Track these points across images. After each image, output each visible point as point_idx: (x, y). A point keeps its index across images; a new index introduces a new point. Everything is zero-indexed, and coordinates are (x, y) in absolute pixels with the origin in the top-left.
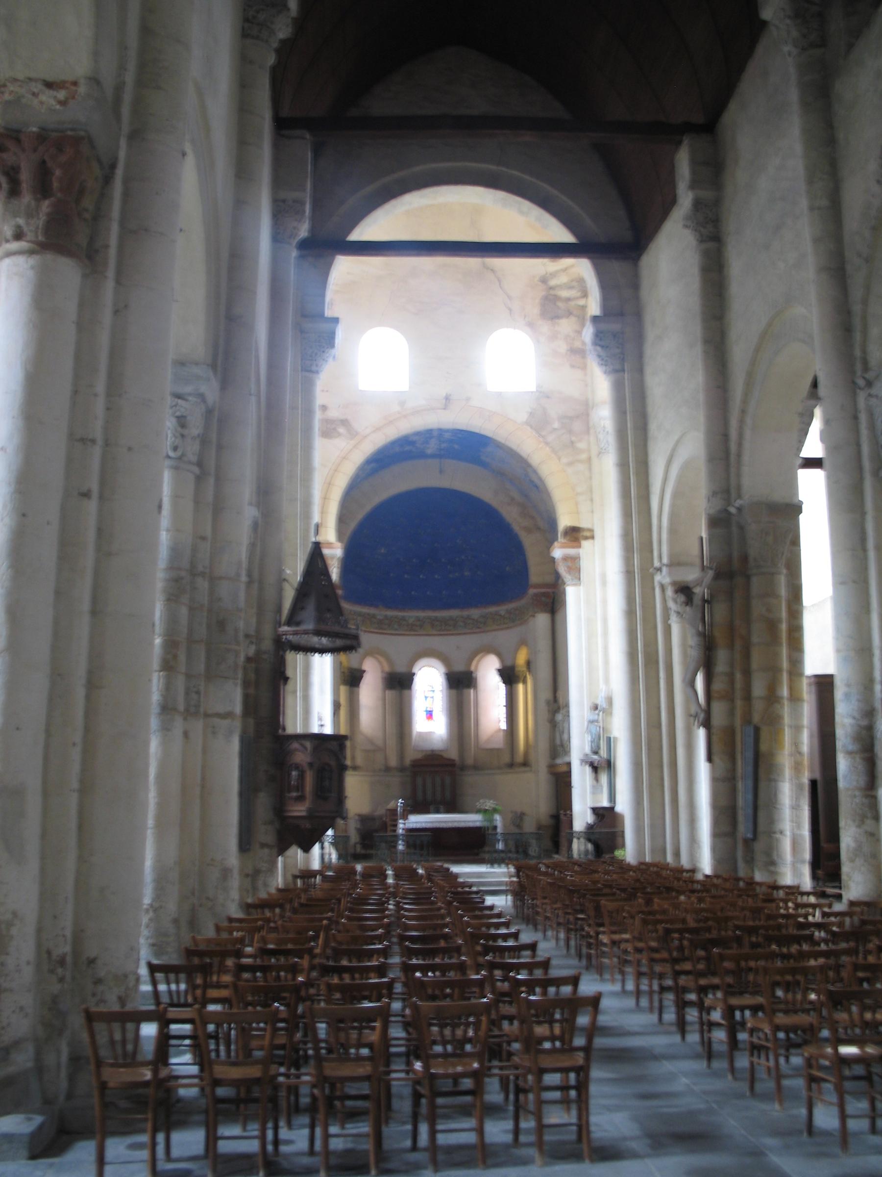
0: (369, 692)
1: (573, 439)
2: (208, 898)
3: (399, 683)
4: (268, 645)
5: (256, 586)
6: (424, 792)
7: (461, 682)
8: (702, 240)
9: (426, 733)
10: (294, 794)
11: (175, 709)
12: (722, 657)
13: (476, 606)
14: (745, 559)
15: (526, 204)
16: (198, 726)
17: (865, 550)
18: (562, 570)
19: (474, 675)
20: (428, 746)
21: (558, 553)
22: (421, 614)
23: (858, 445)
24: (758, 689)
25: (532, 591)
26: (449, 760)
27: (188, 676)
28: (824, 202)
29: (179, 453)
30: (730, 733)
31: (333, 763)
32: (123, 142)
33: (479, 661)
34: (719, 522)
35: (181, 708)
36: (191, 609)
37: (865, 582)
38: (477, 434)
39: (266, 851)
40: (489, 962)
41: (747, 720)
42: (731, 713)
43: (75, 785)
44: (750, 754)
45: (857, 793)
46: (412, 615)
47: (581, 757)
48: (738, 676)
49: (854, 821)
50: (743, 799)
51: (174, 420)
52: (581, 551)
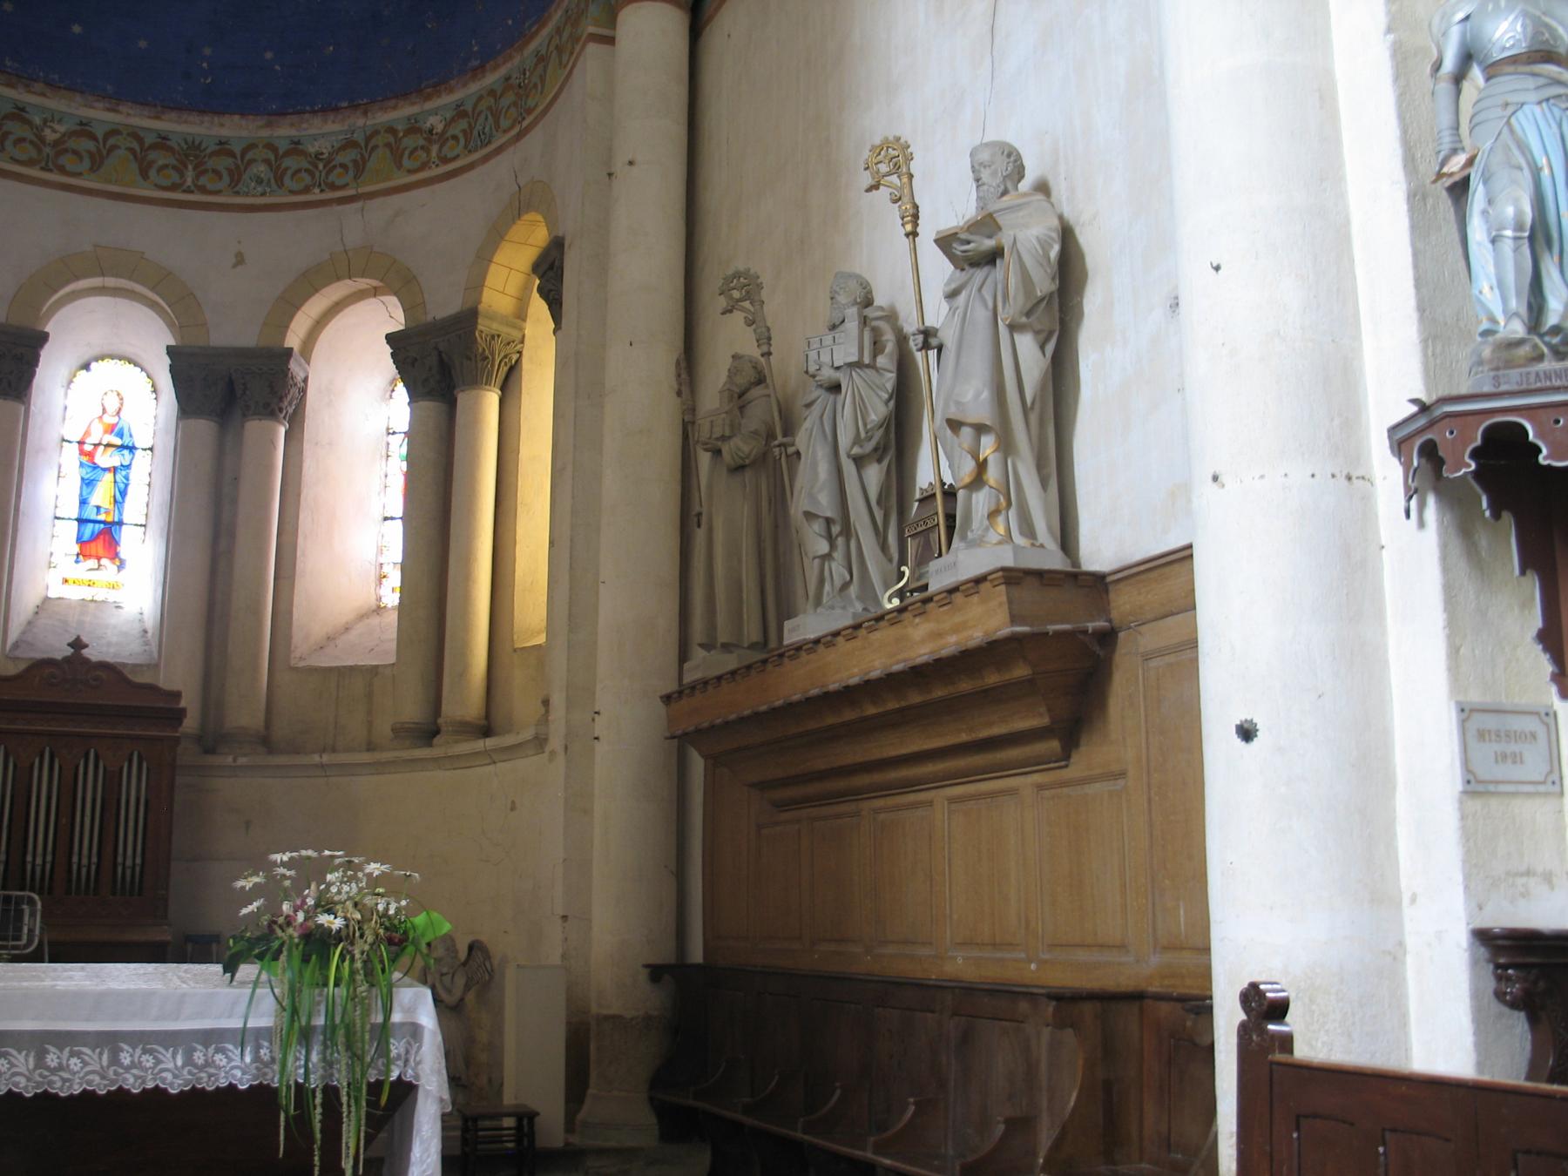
7: (236, 393)
13: (329, 109)
22: (100, 115)
26: (153, 689)
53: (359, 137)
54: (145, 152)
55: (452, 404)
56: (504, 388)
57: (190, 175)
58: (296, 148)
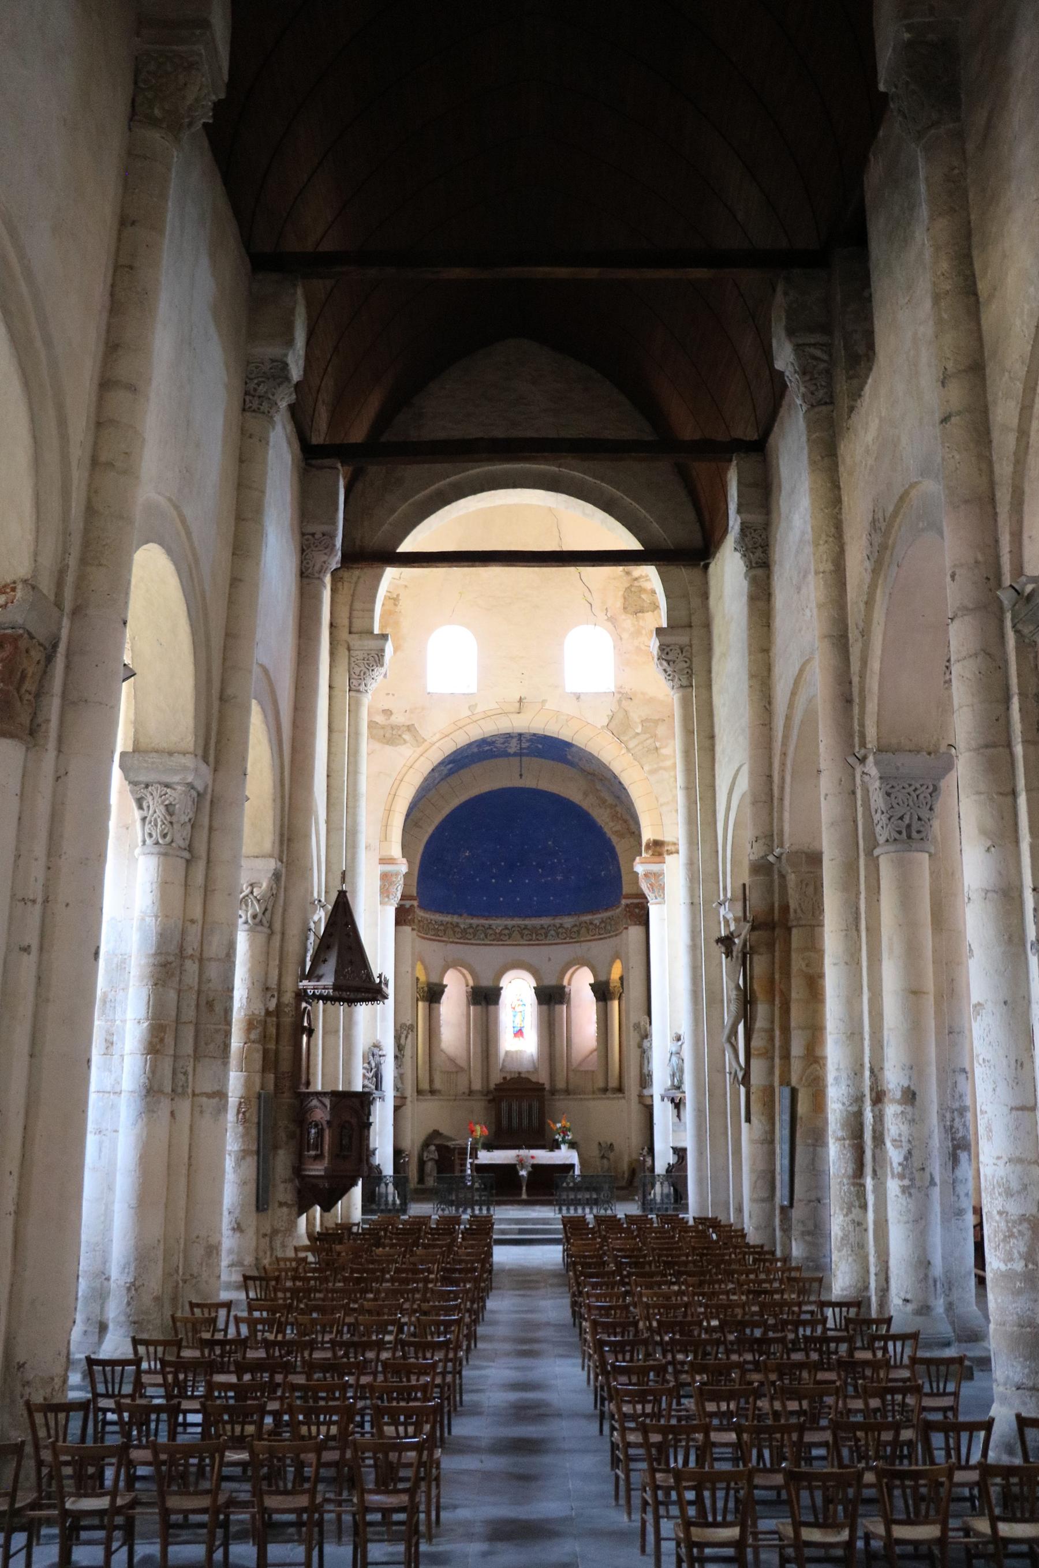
0: (453, 1007)
1: (658, 744)
2: (191, 1275)
3: (485, 997)
4: (288, 997)
5: (277, 938)
6: (520, 1119)
7: (551, 997)
8: (750, 566)
9: (516, 1052)
10: (313, 1153)
11: (161, 1091)
12: (761, 1010)
13: (569, 914)
14: (785, 908)
15: (589, 507)
16: (185, 1106)
17: (858, 930)
18: (644, 886)
19: (567, 990)
20: (515, 1067)
21: (639, 868)
22: (510, 922)
23: (855, 821)
24: (797, 1049)
25: (624, 902)
26: (538, 1083)
27: (175, 1057)
28: (829, 567)
29: (168, 839)
30: (769, 1092)
31: (354, 1121)
32: (66, 622)
34: (762, 868)
35: (168, 1089)
36: (179, 992)
37: (859, 963)
38: (556, 739)
39: (285, 1210)
41: (785, 1081)
42: (771, 1071)
43: (12, 1208)
44: (786, 1117)
45: (845, 1181)
46: (499, 923)
47: (663, 1092)
48: (777, 1033)
49: (842, 1209)
50: (781, 1162)
51: (163, 809)
52: (665, 866)
54: (522, 931)
56: (620, 999)
58: (561, 926)
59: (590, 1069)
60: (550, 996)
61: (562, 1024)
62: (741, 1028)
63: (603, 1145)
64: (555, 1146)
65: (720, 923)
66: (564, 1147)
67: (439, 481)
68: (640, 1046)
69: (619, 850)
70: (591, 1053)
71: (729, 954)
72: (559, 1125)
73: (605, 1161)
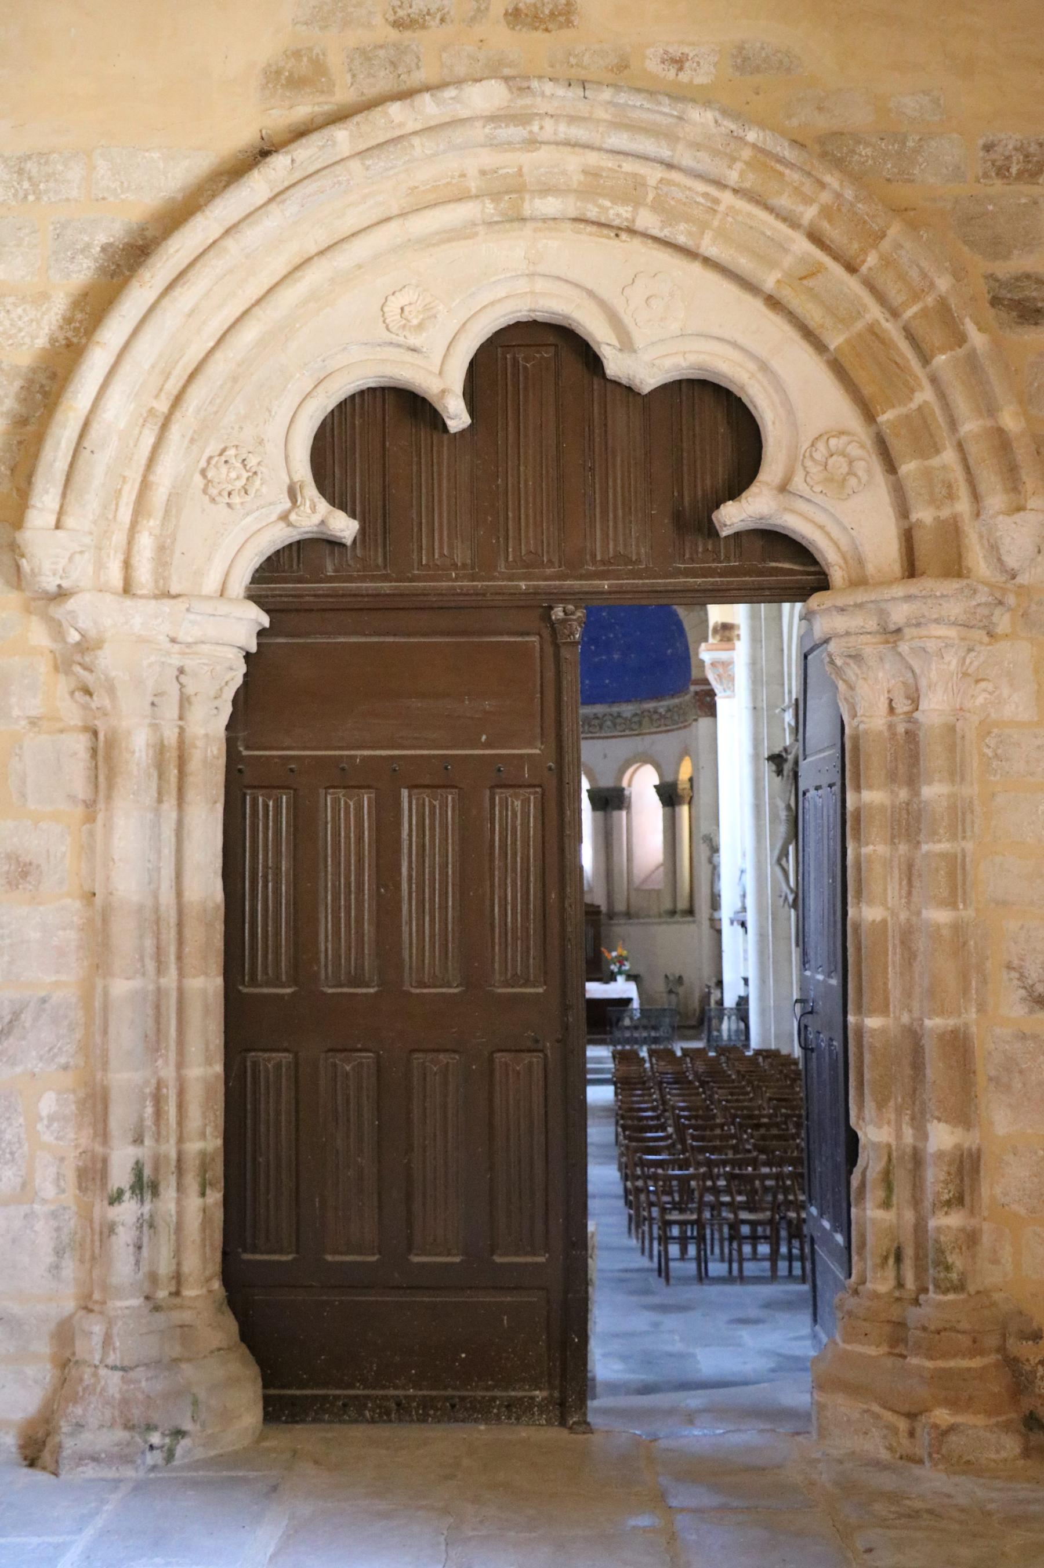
13: (628, 701)
18: (711, 676)
19: (626, 793)
25: (693, 688)
33: (638, 768)
40: (726, 1173)
47: (732, 915)
53: (638, 712)
55: (674, 811)
56: (690, 803)
57: (586, 727)
58: (619, 715)
59: (656, 887)
60: (607, 800)
61: (621, 834)
62: (791, 848)
63: (671, 978)
64: (611, 978)
65: (784, 730)
66: (620, 979)
67: (530, 994)
68: (710, 861)
69: (687, 626)
70: (657, 868)
71: (779, 772)
72: (614, 954)
73: (673, 996)
